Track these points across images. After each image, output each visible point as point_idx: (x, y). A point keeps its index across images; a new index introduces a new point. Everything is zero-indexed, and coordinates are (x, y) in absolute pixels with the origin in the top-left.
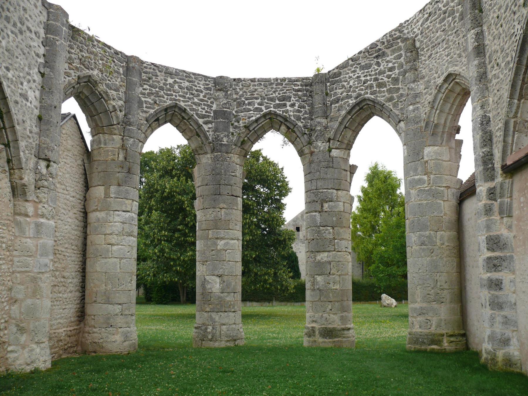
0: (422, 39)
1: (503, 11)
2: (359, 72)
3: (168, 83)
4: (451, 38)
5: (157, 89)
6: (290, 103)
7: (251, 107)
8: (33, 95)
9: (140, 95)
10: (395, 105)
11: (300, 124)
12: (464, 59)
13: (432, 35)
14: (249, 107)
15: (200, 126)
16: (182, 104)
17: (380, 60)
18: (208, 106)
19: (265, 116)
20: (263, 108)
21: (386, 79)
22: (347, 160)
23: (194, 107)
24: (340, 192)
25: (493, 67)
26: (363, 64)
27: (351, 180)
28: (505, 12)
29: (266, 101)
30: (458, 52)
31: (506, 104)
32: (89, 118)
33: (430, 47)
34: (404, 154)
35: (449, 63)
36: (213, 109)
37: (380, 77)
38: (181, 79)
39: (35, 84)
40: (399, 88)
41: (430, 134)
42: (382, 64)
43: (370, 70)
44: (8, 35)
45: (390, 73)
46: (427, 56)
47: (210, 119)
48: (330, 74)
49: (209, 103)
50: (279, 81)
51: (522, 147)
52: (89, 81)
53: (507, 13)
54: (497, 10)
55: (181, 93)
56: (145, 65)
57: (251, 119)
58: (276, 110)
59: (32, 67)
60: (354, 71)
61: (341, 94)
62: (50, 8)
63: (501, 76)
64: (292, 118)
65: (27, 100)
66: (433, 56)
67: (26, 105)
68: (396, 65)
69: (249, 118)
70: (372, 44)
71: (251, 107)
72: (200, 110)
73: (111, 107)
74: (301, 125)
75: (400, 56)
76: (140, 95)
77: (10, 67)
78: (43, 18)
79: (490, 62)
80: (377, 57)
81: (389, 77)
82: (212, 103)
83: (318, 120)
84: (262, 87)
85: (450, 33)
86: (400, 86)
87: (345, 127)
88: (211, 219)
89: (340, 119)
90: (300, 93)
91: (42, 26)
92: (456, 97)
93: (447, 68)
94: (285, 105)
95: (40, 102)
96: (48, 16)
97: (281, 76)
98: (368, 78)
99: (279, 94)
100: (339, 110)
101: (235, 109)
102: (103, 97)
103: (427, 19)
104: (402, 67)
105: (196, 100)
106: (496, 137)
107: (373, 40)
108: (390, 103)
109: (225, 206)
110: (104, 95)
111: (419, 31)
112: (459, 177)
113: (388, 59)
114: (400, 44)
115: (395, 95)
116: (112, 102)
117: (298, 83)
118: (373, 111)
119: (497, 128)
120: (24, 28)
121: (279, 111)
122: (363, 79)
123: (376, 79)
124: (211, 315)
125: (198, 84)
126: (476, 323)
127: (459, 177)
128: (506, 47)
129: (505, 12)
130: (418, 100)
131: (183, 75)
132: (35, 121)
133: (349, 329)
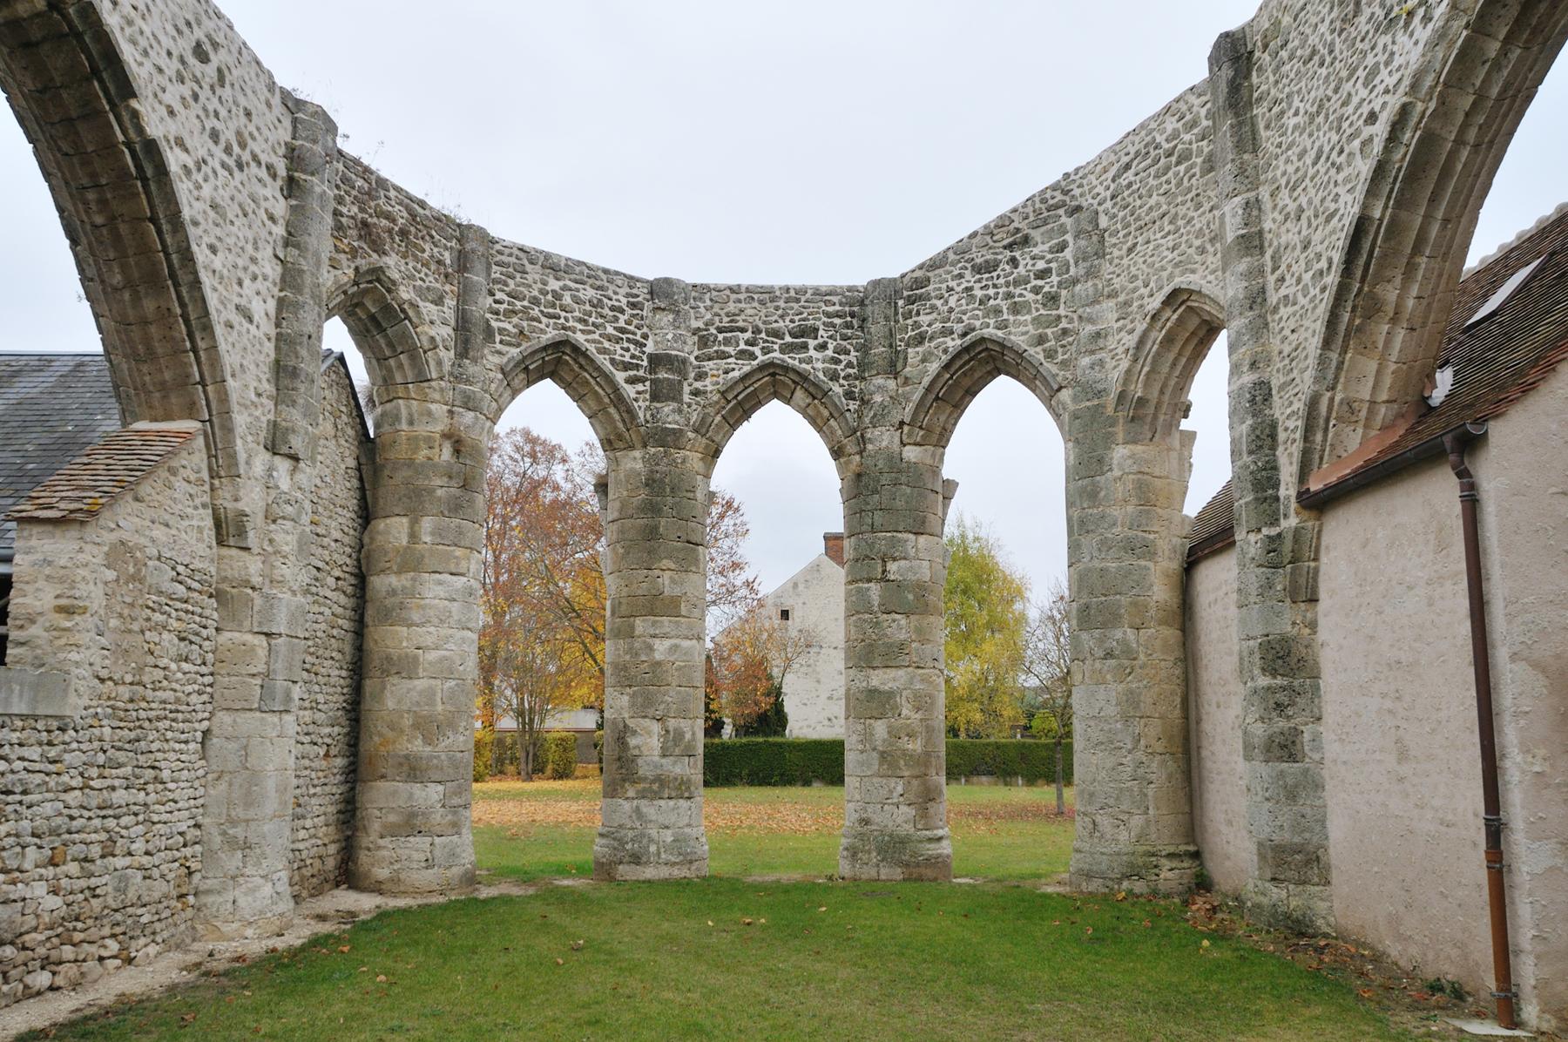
1: (1309, 161)
3: (548, 288)
4: (1182, 210)
5: (526, 303)
7: (730, 350)
8: (264, 308)
9: (488, 316)
10: (1050, 355)
11: (837, 389)
12: (1210, 259)
15: (616, 389)
16: (580, 338)
17: (1017, 254)
18: (636, 343)
19: (762, 368)
20: (757, 350)
21: (1030, 296)
22: (935, 471)
23: (607, 344)
24: (922, 539)
25: (1282, 279)
26: (978, 261)
27: (945, 514)
28: (1315, 164)
29: (763, 335)
30: (1197, 243)
31: (1312, 362)
32: (374, 362)
33: (1132, 228)
34: (1067, 460)
35: (1177, 265)
36: (648, 350)
37: (1018, 291)
38: (576, 282)
39: (267, 284)
40: (1059, 317)
41: (1121, 423)
42: (1022, 263)
43: (994, 274)
44: (215, 172)
45: (1040, 283)
46: (1125, 248)
47: (641, 373)
50: (792, 293)
51: (1345, 455)
52: (379, 280)
53: (1319, 166)
54: (1295, 158)
55: (576, 314)
56: (497, 247)
57: (731, 375)
58: (786, 357)
59: (260, 244)
60: (961, 276)
62: (299, 110)
63: (1302, 301)
64: (821, 375)
65: (251, 321)
66: (1139, 248)
67: (248, 331)
68: (1053, 265)
69: (726, 372)
70: (1001, 217)
71: (730, 350)
72: (620, 351)
73: (425, 340)
74: (840, 391)
75: (1062, 247)
76: (488, 316)
77: (218, 244)
78: (284, 134)
79: (1274, 270)
80: (1010, 247)
81: (1036, 290)
82: (645, 336)
83: (879, 381)
84: (756, 304)
85: (1180, 199)
86: (1062, 312)
87: (937, 398)
88: (640, 592)
89: (926, 381)
90: (837, 321)
91: (282, 151)
92: (1188, 340)
93: (1171, 277)
94: (805, 347)
95: (278, 325)
96: (295, 127)
97: (795, 281)
98: (991, 292)
99: (792, 321)
100: (923, 361)
101: (696, 353)
102: (407, 317)
103: (1127, 167)
104: (1068, 271)
105: (610, 330)
106: (1286, 429)
107: (1003, 208)
108: (1039, 349)
109: (673, 566)
110: (411, 313)
111: (1108, 193)
112: (1185, 512)
113: (1036, 251)
114: (1064, 219)
115: (1049, 331)
116: (426, 328)
117: (835, 299)
118: (1001, 367)
119: (1289, 411)
120: (246, 157)
121: (792, 360)
122: (978, 293)
123: (1009, 296)
125: (616, 293)
126: (1224, 829)
127: (1185, 512)
128: (1316, 238)
129: (1315, 164)
130: (1101, 343)
131: (582, 273)
132: (265, 373)
133: (940, 839)
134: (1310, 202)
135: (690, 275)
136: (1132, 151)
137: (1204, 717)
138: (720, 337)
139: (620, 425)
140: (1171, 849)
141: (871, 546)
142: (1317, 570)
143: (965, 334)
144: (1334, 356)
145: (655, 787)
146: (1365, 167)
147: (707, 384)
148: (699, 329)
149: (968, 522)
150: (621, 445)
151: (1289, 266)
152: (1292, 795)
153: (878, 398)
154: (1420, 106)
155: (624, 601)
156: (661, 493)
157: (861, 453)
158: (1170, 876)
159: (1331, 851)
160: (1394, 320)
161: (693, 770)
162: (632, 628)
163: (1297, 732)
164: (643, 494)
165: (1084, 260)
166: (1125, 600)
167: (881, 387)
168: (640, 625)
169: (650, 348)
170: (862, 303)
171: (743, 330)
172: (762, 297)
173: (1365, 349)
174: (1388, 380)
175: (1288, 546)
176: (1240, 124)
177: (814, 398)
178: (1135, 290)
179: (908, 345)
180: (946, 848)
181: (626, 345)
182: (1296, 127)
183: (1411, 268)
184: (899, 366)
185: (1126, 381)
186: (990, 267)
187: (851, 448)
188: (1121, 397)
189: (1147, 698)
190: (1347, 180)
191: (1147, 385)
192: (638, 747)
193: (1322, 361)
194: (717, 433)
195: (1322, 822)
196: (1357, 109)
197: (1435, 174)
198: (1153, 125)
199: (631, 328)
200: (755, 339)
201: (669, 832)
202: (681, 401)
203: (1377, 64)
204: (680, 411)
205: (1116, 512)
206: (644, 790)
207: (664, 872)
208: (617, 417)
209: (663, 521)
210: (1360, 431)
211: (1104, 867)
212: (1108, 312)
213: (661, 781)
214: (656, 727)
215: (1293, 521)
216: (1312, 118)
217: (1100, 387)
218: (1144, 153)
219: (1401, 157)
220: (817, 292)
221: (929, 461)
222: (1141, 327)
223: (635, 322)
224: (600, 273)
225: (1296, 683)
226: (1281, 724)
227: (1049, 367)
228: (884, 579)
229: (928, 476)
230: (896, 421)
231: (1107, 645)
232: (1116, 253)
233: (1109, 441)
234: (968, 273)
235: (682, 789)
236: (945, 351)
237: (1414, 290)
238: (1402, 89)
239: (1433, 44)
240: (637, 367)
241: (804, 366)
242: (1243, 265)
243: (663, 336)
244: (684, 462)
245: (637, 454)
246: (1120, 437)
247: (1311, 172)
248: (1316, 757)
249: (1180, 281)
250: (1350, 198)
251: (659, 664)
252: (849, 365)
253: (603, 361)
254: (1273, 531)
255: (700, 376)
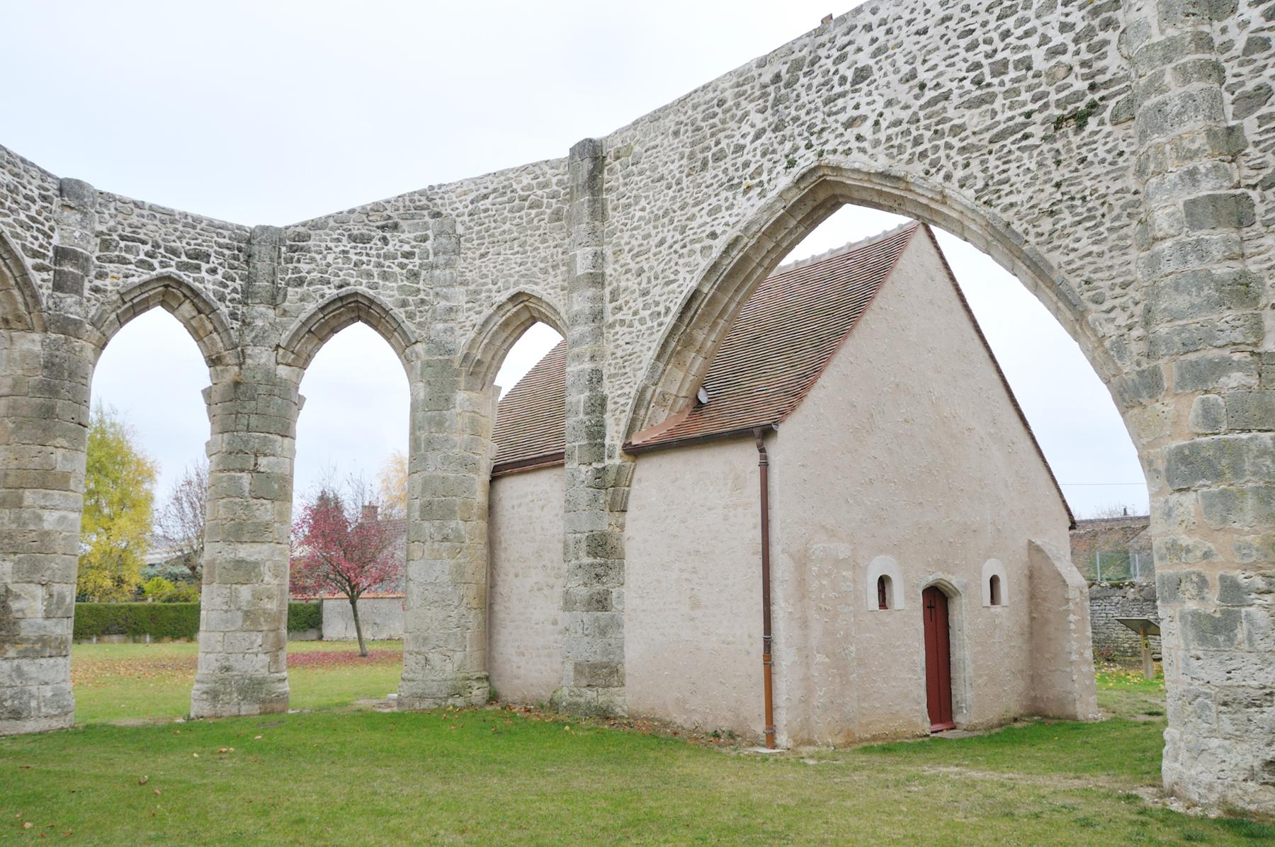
0: (472, 224)
2: (346, 244)
6: (208, 266)
7: (130, 257)
10: (411, 316)
12: (551, 279)
13: (493, 225)
14: (127, 256)
15: (24, 273)
17: (388, 235)
18: (44, 234)
19: (159, 279)
20: (155, 263)
21: (397, 269)
23: (19, 230)
29: (162, 250)
30: (542, 265)
35: (523, 276)
37: (387, 263)
40: (419, 290)
42: (391, 243)
46: (478, 253)
47: (47, 262)
48: (289, 232)
49: (46, 229)
50: (190, 220)
53: (662, 248)
57: (130, 280)
58: (182, 274)
60: (339, 240)
61: (308, 273)
66: (490, 256)
68: (417, 250)
69: (126, 277)
70: (377, 204)
72: (30, 239)
75: (425, 239)
80: (382, 228)
82: (52, 229)
83: (261, 308)
84: (157, 222)
86: (421, 286)
87: (310, 331)
88: (32, 466)
89: (303, 316)
90: (226, 252)
93: (516, 283)
94: (198, 268)
97: (194, 210)
100: (301, 300)
101: (97, 253)
105: (23, 217)
107: (380, 197)
108: (402, 310)
109: (65, 444)
111: (466, 211)
114: (427, 219)
115: (410, 298)
118: (362, 314)
121: (187, 277)
122: (354, 258)
124: (18, 667)
125: (30, 183)
128: (653, 292)
130: (453, 315)
134: (651, 268)
135: (99, 180)
136: (491, 187)
137: (500, 583)
138: (122, 244)
139: (22, 308)
140: (478, 675)
141: (246, 443)
142: (628, 493)
143: (341, 287)
144: (661, 366)
145: (38, 647)
146: (705, 264)
147: (107, 283)
148: (102, 233)
149: (106, 409)
150: (19, 326)
151: (627, 303)
152: (603, 632)
153: (259, 323)
154: (746, 240)
155: (12, 473)
156: (59, 376)
157: (240, 365)
158: (478, 693)
159: (626, 665)
160: (698, 352)
161: (65, 629)
162: (21, 499)
163: (608, 592)
164: (40, 376)
165: (444, 253)
166: (458, 500)
167: (262, 314)
168: (29, 497)
169: (56, 241)
170: (249, 242)
171: (144, 242)
172: (164, 217)
173: (679, 364)
174: (687, 385)
175: (611, 477)
176: (595, 201)
177: (200, 312)
178: (485, 284)
179: (288, 284)
180: (286, 687)
181: (35, 234)
182: (641, 218)
183: (715, 324)
184: (279, 299)
185: (471, 347)
186: (365, 239)
187: (230, 358)
188: (466, 357)
189: (469, 570)
190: (686, 265)
191: (484, 351)
192: (22, 610)
193: (653, 368)
194: (109, 328)
195: (621, 648)
196: (700, 227)
197: (742, 278)
198: (511, 175)
199: (41, 219)
200: (154, 253)
201: (48, 688)
202: (81, 295)
203: (720, 207)
204: (81, 304)
205: (456, 438)
206: (26, 650)
207: (43, 725)
208: (20, 299)
209: (60, 403)
210: (667, 412)
211: (435, 690)
212: (459, 296)
213: (44, 641)
214: (40, 592)
215: (617, 461)
216: (657, 218)
217: (451, 347)
218: (502, 192)
219: (728, 265)
220: (211, 223)
221: (294, 379)
222: (487, 312)
223: (45, 214)
224: (18, 161)
225: (609, 562)
226: (598, 587)
227: (409, 325)
228: (255, 470)
229: (293, 390)
230: (274, 344)
231: (445, 531)
232: (470, 254)
233: (454, 386)
234: (345, 239)
235: (59, 649)
236: (322, 296)
237: (713, 337)
238: (738, 227)
239: (763, 210)
240: (44, 256)
241: (197, 284)
242: (590, 292)
243: (71, 231)
244: (81, 351)
245: (37, 337)
246: (462, 385)
247: (654, 250)
248: (620, 607)
249: (523, 287)
250: (689, 277)
251: (47, 533)
252: (235, 290)
253: (15, 244)
254: (600, 466)
255: (101, 275)
